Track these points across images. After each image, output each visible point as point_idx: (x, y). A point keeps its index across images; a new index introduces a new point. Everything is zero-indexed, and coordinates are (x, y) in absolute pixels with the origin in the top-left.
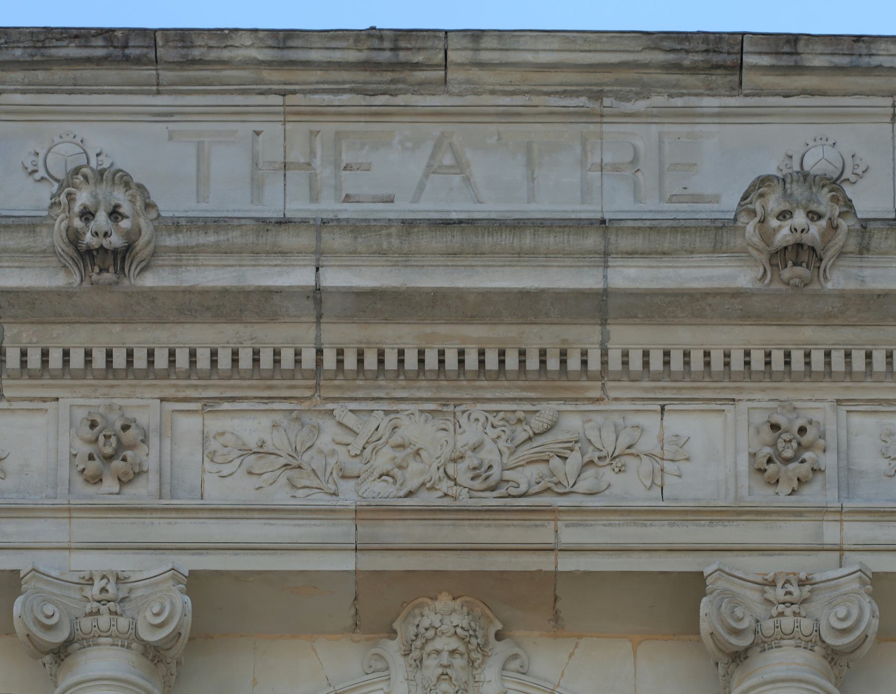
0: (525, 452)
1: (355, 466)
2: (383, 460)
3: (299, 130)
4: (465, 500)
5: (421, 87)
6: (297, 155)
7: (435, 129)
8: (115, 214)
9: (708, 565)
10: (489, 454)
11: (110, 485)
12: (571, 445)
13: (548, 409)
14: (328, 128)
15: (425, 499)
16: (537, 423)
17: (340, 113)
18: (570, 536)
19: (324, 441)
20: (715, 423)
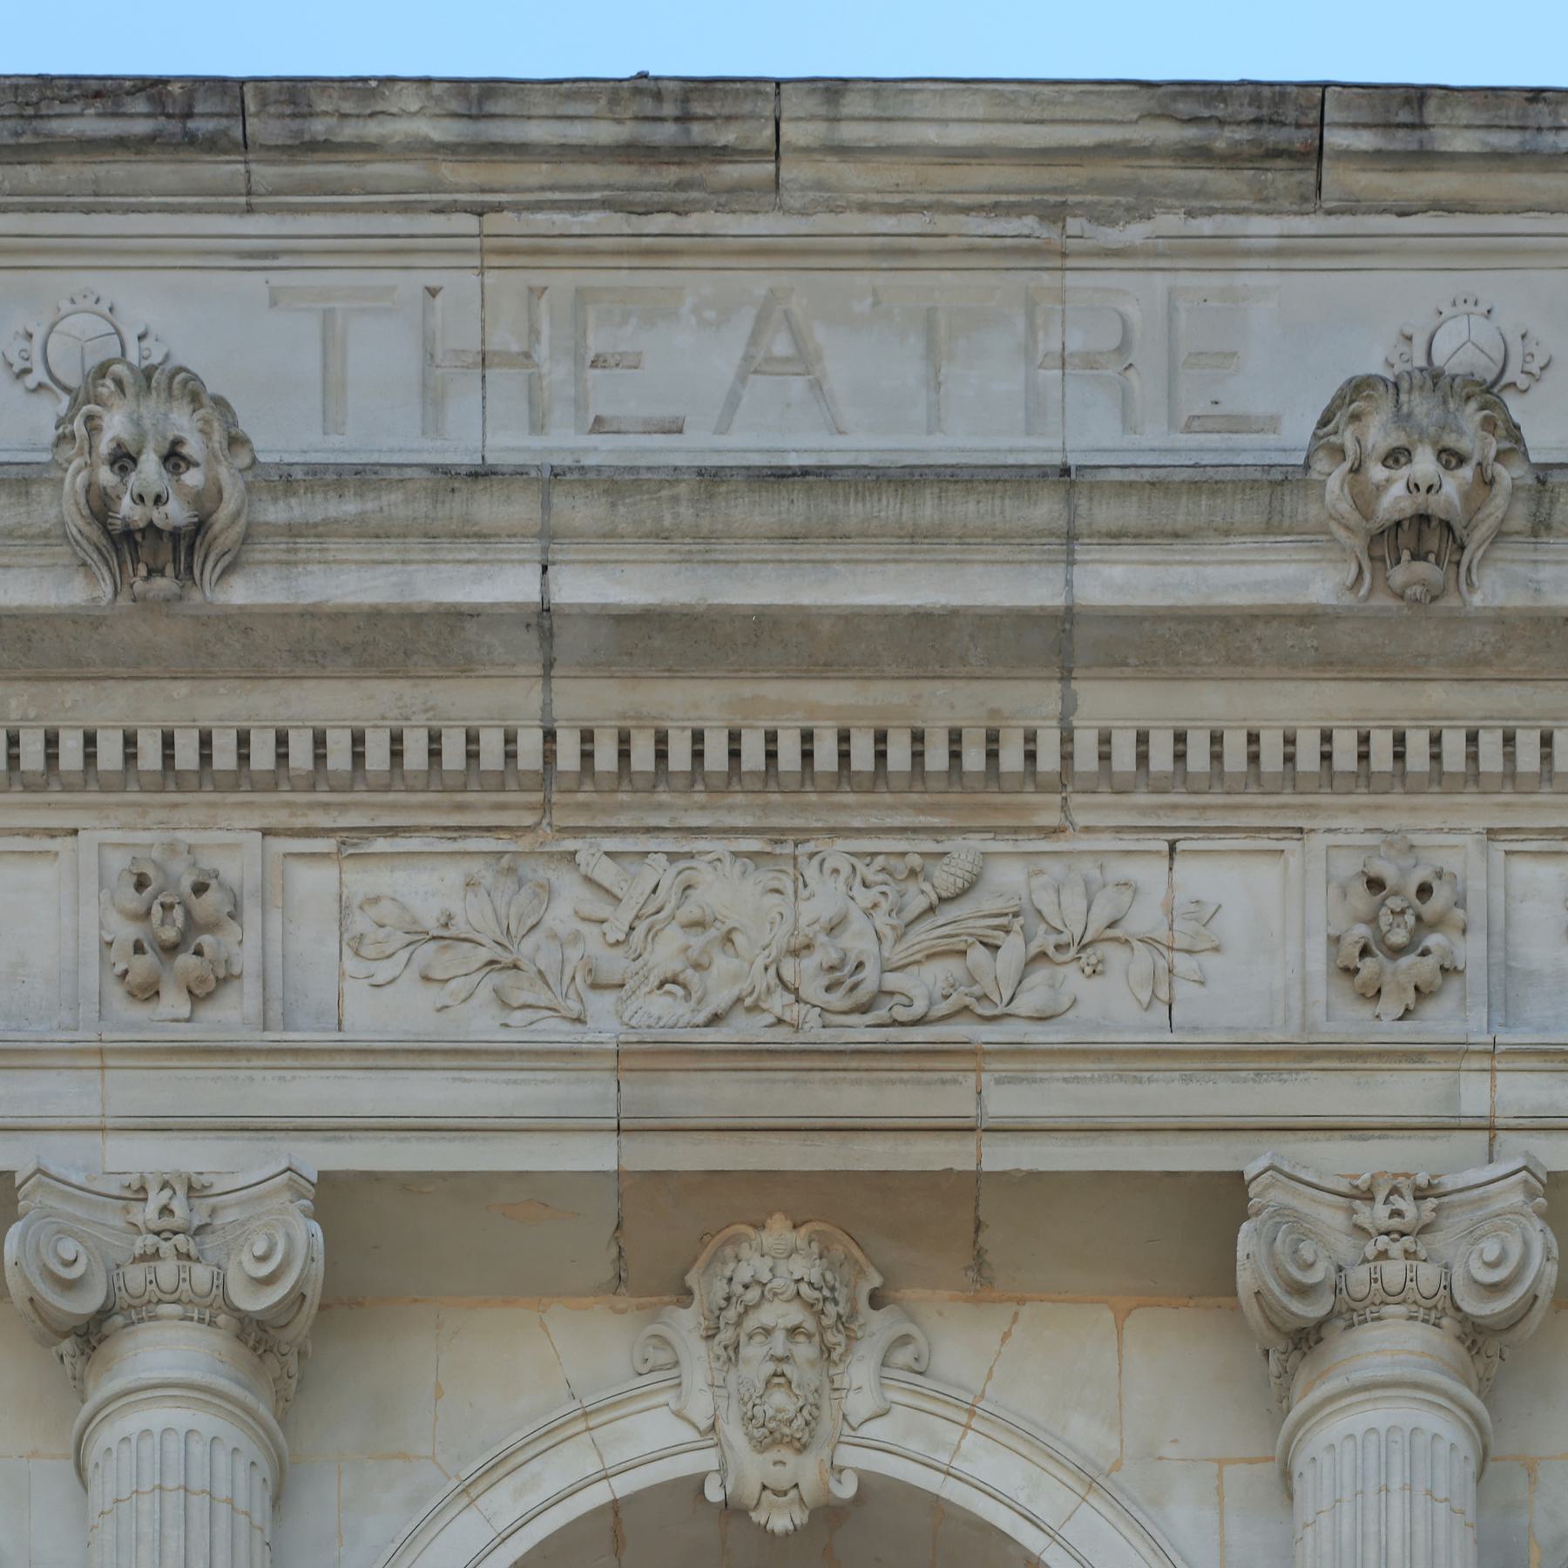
0: (923, 936)
1: (614, 964)
2: (666, 953)
3: (508, 284)
4: (814, 1033)
5: (733, 198)
6: (505, 338)
7: (758, 283)
8: (174, 458)
9: (1252, 1158)
10: (858, 941)
11: (174, 1003)
12: (1007, 920)
13: (964, 849)
14: (562, 281)
15: (744, 1029)
16: (945, 878)
17: (584, 251)
18: (1004, 1102)
19: (560, 915)
20: (1266, 873)
